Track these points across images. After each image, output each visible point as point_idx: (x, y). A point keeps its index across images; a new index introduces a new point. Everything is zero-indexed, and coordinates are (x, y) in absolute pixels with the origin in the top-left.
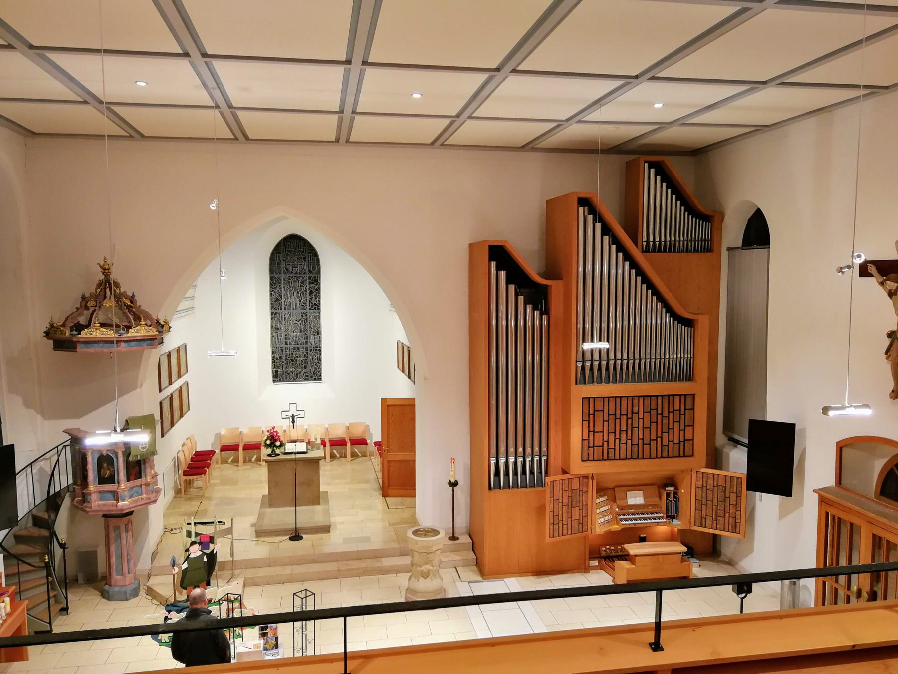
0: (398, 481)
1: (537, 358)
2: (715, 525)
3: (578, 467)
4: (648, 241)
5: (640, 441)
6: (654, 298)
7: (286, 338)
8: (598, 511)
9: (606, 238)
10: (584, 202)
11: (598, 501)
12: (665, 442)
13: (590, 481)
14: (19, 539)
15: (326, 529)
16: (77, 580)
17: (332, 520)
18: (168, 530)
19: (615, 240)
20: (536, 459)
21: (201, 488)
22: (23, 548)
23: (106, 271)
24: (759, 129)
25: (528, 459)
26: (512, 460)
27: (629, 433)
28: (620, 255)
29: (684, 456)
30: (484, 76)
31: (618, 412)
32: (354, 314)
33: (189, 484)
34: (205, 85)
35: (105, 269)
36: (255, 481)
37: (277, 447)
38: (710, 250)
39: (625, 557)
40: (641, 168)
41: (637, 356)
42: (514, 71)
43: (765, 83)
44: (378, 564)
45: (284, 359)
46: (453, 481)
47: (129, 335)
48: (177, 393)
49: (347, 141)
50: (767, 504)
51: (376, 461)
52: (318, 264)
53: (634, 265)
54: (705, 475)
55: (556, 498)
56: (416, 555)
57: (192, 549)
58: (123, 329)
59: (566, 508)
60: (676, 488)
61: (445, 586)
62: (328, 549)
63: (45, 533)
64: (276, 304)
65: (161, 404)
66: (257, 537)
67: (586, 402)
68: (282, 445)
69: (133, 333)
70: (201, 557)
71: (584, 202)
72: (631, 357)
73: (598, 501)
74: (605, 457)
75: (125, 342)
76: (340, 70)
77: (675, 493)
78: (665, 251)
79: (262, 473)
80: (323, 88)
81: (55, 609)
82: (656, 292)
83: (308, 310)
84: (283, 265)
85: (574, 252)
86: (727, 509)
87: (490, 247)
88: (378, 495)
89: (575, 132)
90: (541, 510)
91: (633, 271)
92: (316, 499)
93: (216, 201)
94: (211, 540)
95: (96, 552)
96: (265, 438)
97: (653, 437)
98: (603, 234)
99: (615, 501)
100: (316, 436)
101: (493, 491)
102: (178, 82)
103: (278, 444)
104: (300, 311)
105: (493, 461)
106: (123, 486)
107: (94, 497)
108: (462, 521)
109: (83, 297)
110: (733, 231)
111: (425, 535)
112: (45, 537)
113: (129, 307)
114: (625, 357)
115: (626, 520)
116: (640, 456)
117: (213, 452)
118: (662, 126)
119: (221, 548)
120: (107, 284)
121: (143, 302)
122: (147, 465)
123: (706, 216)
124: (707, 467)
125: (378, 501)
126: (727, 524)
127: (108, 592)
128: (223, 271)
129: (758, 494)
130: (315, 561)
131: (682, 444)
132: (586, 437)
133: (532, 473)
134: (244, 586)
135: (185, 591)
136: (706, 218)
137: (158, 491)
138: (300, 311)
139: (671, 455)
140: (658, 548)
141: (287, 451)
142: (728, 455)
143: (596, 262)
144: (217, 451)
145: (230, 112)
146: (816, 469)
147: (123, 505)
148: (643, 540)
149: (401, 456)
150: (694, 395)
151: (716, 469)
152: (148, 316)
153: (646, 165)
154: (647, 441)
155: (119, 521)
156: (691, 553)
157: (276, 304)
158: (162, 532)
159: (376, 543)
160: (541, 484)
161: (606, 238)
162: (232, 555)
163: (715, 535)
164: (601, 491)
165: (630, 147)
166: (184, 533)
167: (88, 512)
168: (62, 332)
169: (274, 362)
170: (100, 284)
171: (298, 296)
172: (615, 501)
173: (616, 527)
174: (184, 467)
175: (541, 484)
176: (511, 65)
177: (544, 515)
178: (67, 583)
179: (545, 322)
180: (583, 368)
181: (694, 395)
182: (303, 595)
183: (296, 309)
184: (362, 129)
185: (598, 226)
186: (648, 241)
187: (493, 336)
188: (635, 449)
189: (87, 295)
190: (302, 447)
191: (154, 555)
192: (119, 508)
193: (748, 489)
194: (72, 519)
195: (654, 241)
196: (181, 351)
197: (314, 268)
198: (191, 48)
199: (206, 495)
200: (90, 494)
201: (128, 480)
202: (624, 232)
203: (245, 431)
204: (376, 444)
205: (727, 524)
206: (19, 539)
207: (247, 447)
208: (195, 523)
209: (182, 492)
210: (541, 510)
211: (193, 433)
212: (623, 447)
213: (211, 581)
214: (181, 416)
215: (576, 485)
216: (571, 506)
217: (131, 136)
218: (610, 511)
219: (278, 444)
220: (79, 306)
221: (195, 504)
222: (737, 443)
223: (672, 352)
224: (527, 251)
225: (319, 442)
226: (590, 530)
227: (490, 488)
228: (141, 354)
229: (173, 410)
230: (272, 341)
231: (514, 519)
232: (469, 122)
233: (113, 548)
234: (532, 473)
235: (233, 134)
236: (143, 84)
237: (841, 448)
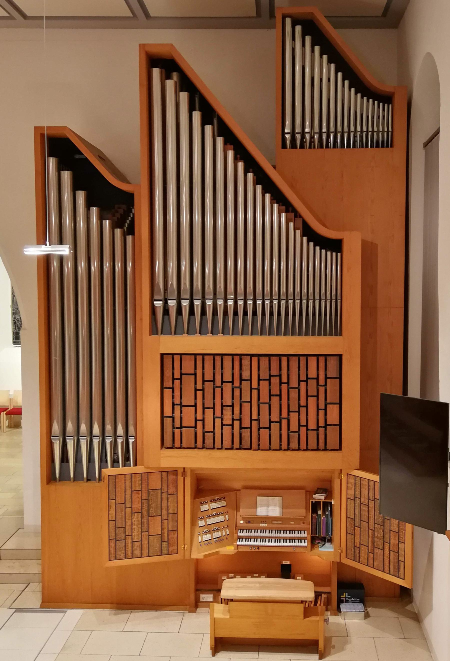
2: (371, 562)
3: (159, 459)
5: (255, 423)
12: (294, 426)
13: (180, 479)
31: (218, 378)
54: (358, 479)
55: (118, 501)
59: (137, 517)
86: (387, 536)
97: (275, 417)
115: (248, 539)
124: (362, 468)
126: (387, 562)
131: (321, 430)
133: (78, 460)
136: (385, 98)
154: (264, 422)
161: (208, 129)
172: (237, 509)
188: (246, 434)
205: (387, 562)
215: (155, 482)
216: (146, 514)
237: (340, 449)
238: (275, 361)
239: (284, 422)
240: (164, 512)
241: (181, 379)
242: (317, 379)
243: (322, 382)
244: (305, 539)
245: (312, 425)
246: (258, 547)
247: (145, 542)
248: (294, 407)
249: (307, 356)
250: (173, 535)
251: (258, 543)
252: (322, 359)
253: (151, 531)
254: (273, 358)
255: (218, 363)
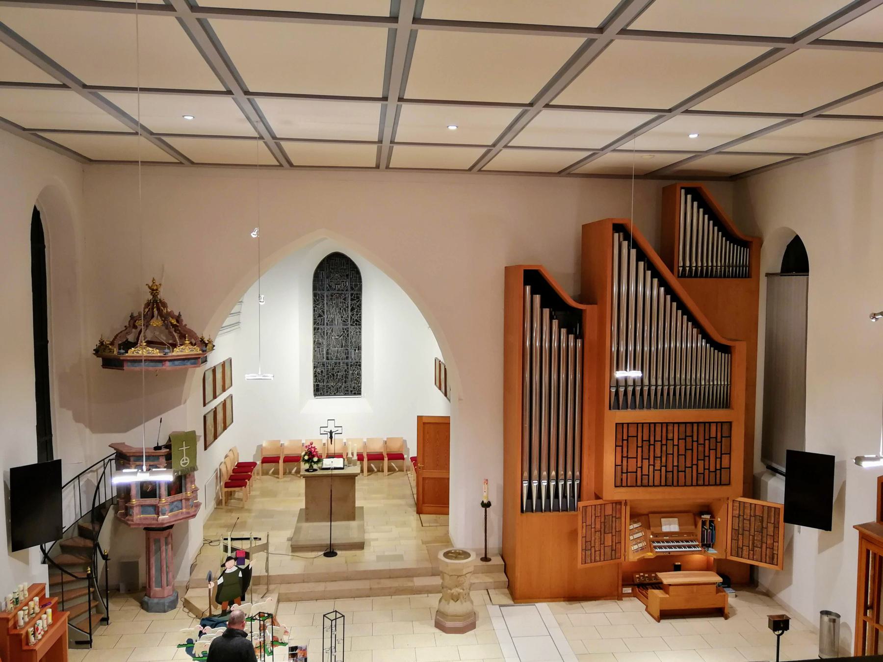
0: (433, 498)
1: (571, 377)
2: (751, 556)
3: (611, 493)
4: (684, 267)
5: (675, 468)
6: (690, 324)
7: (327, 353)
8: (631, 538)
9: (641, 264)
10: (619, 228)
11: (631, 527)
12: (701, 470)
13: (623, 507)
14: (65, 549)
15: (360, 546)
16: (118, 590)
17: (367, 536)
18: (208, 542)
19: (650, 266)
20: (569, 483)
21: (241, 500)
22: (68, 558)
23: (154, 291)
24: (796, 157)
25: (561, 483)
26: (544, 483)
27: (664, 459)
28: (656, 281)
29: (720, 484)
30: (517, 111)
32: (394, 331)
33: (229, 495)
34: (248, 118)
35: (153, 290)
36: (293, 494)
37: (315, 463)
38: (748, 276)
39: (659, 585)
40: (678, 196)
41: (672, 382)
42: (547, 106)
43: (802, 115)
44: (410, 584)
45: (325, 373)
46: (485, 501)
47: (174, 354)
48: (221, 406)
49: (387, 167)
50: (805, 537)
51: (412, 476)
52: (361, 282)
53: (669, 291)
56: (447, 577)
57: (228, 564)
58: (169, 348)
59: (598, 534)
60: (713, 516)
61: (476, 609)
62: (362, 567)
63: (89, 543)
64: (319, 320)
65: (205, 417)
66: (293, 551)
67: (620, 427)
68: (319, 461)
69: (177, 352)
70: (236, 572)
71: (619, 228)
72: (666, 383)
73: (631, 527)
74: (639, 483)
75: (170, 361)
76: (378, 105)
77: (711, 522)
78: (701, 276)
79: (300, 485)
80: (364, 121)
81: (96, 619)
82: (691, 318)
83: (349, 326)
84: (326, 282)
85: (609, 279)
86: (764, 539)
87: (525, 271)
88: (413, 511)
89: (610, 159)
90: (573, 534)
91: (669, 297)
92: (351, 514)
93: (257, 230)
94: (247, 555)
95: (137, 563)
96: (303, 453)
97: (689, 464)
98: (638, 260)
99: (649, 528)
100: (354, 448)
101: (524, 515)
102: (224, 116)
103: (315, 459)
104: (341, 326)
105: (526, 484)
106: (163, 500)
107: (136, 510)
108: (494, 542)
109: (132, 317)
110: (771, 258)
111: (456, 558)
112: (90, 548)
113: (174, 326)
114: (660, 382)
115: (660, 547)
116: (675, 483)
117: (254, 464)
118: (698, 154)
119: (256, 564)
120: (156, 305)
121: (189, 322)
122: (188, 480)
123: (744, 240)
124: (744, 496)
125: (412, 518)
127: (147, 603)
128: (262, 296)
129: (796, 526)
130: (347, 579)
131: (718, 472)
132: (619, 463)
133: (564, 496)
134: (279, 601)
135: (220, 606)
136: (744, 244)
137: (198, 506)
138: (341, 326)
139: (707, 483)
140: (693, 578)
141: (324, 466)
142: (766, 484)
143: (630, 285)
144: (259, 463)
145: (276, 142)
146: (857, 506)
147: (163, 519)
148: (678, 568)
149: (436, 474)
150: (730, 423)
151: (754, 497)
152: (192, 335)
153: (683, 191)
154: (682, 468)
155: (160, 535)
156: (728, 582)
157: (319, 320)
158: (201, 546)
159: (410, 561)
160: (573, 508)
161: (641, 264)
162: (267, 571)
163: (752, 566)
164: (635, 516)
165: (668, 172)
166: (222, 548)
167: (129, 525)
168: (111, 351)
169: (315, 376)
170: (148, 305)
171: (340, 313)
172: (649, 528)
173: (650, 555)
174: (225, 478)
175: (573, 508)
176: (544, 99)
177: (576, 540)
178: (109, 592)
179: (579, 344)
180: (617, 392)
181: (730, 423)
182: (332, 616)
183: (338, 325)
184: (400, 156)
185: (633, 252)
186: (684, 267)
187: (527, 356)
188: (670, 475)
189: (135, 314)
190: (338, 462)
191: (193, 567)
192: (160, 521)
193: (786, 521)
194: (115, 531)
195: (690, 267)
196: (226, 365)
197: (356, 285)
198: (233, 85)
199: (246, 507)
200: (132, 507)
201: (169, 494)
202: (660, 257)
203: (286, 444)
204: (413, 459)
206: (65, 549)
207: (289, 460)
208: (232, 539)
209: (223, 503)
210: (573, 534)
211: (235, 445)
212: (657, 473)
213: (246, 596)
214: (225, 428)
215: (609, 510)
216: (603, 531)
217: (181, 163)
218: (645, 538)
219: (315, 459)
220: (127, 324)
221: (235, 515)
222: (775, 471)
223: (709, 373)
224: (562, 275)
225: (355, 457)
226: (623, 557)
227: (522, 511)
228: (186, 370)
229: (217, 422)
230: (314, 356)
231: (545, 542)
232: (505, 151)
233: (153, 561)
234: (564, 496)
235: (278, 161)
236: (190, 118)
238: (689, 426)
239: (695, 467)
240: (614, 531)
241: (627, 440)
242: (716, 438)
243: (719, 440)
244: (697, 546)
245: (712, 469)
246: (669, 552)
247: (602, 551)
248: (701, 457)
249: (710, 423)
250: (618, 545)
251: (668, 550)
252: (719, 425)
253: (606, 544)
254: (688, 425)
255: (652, 429)
